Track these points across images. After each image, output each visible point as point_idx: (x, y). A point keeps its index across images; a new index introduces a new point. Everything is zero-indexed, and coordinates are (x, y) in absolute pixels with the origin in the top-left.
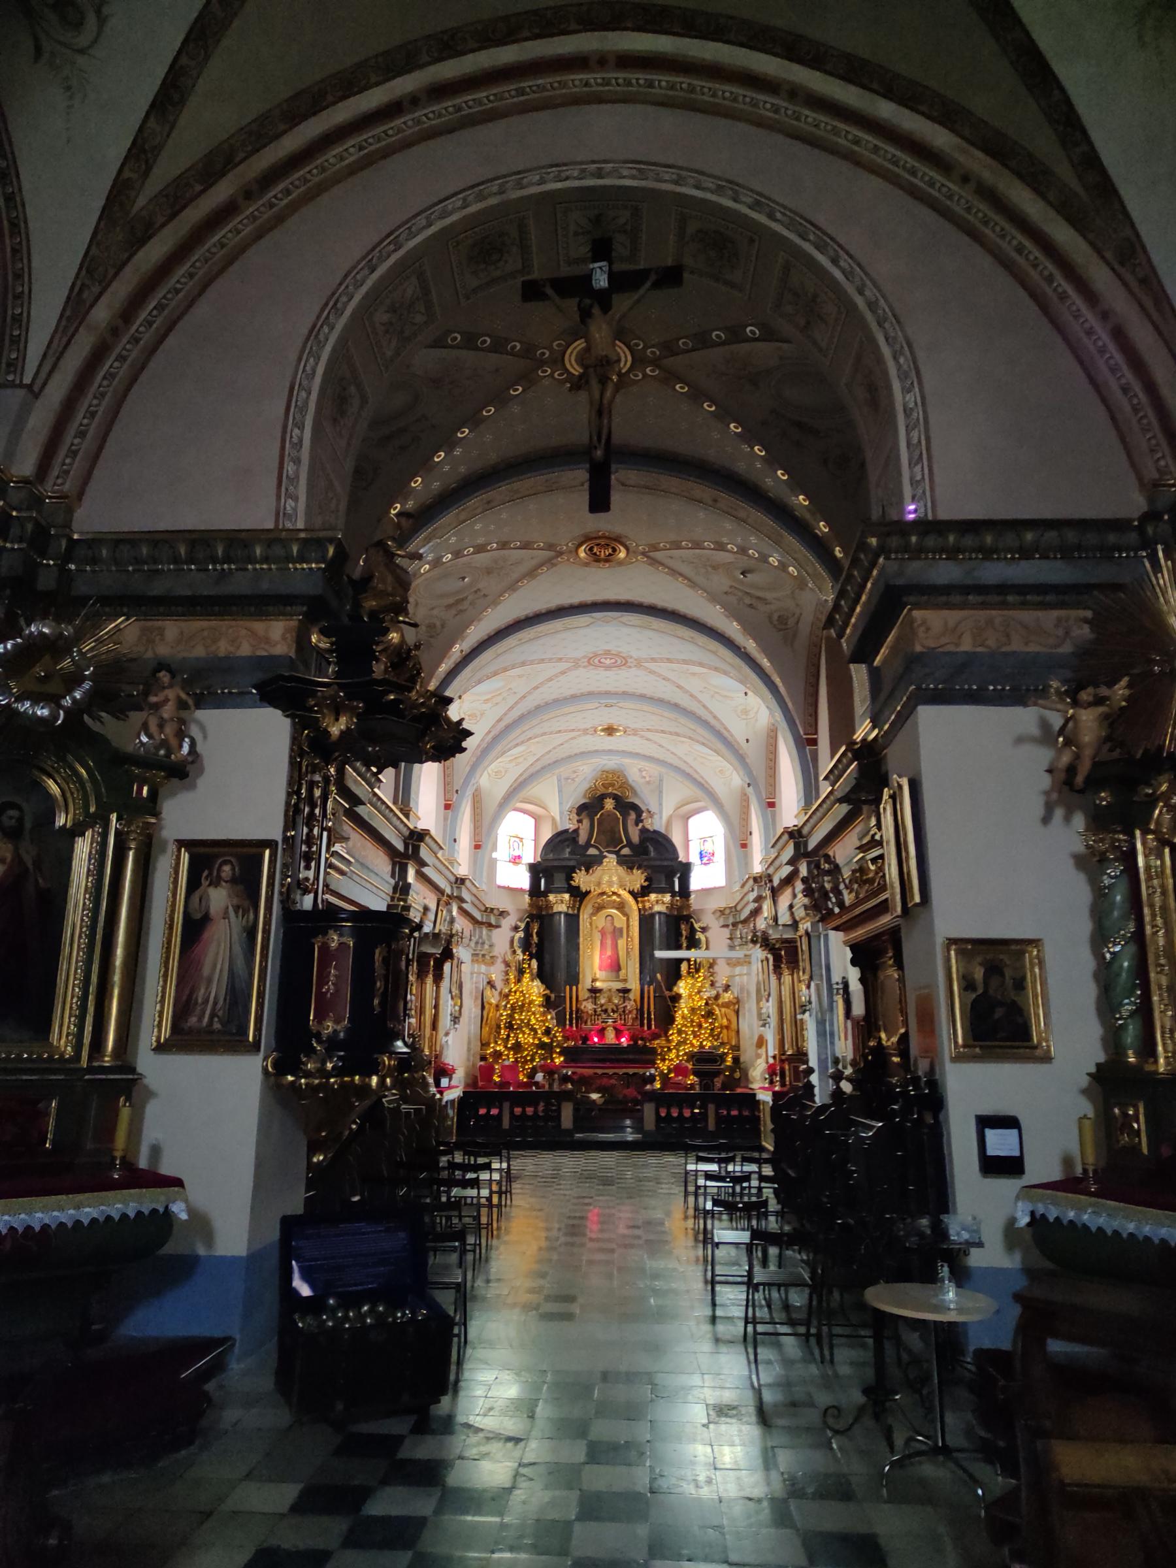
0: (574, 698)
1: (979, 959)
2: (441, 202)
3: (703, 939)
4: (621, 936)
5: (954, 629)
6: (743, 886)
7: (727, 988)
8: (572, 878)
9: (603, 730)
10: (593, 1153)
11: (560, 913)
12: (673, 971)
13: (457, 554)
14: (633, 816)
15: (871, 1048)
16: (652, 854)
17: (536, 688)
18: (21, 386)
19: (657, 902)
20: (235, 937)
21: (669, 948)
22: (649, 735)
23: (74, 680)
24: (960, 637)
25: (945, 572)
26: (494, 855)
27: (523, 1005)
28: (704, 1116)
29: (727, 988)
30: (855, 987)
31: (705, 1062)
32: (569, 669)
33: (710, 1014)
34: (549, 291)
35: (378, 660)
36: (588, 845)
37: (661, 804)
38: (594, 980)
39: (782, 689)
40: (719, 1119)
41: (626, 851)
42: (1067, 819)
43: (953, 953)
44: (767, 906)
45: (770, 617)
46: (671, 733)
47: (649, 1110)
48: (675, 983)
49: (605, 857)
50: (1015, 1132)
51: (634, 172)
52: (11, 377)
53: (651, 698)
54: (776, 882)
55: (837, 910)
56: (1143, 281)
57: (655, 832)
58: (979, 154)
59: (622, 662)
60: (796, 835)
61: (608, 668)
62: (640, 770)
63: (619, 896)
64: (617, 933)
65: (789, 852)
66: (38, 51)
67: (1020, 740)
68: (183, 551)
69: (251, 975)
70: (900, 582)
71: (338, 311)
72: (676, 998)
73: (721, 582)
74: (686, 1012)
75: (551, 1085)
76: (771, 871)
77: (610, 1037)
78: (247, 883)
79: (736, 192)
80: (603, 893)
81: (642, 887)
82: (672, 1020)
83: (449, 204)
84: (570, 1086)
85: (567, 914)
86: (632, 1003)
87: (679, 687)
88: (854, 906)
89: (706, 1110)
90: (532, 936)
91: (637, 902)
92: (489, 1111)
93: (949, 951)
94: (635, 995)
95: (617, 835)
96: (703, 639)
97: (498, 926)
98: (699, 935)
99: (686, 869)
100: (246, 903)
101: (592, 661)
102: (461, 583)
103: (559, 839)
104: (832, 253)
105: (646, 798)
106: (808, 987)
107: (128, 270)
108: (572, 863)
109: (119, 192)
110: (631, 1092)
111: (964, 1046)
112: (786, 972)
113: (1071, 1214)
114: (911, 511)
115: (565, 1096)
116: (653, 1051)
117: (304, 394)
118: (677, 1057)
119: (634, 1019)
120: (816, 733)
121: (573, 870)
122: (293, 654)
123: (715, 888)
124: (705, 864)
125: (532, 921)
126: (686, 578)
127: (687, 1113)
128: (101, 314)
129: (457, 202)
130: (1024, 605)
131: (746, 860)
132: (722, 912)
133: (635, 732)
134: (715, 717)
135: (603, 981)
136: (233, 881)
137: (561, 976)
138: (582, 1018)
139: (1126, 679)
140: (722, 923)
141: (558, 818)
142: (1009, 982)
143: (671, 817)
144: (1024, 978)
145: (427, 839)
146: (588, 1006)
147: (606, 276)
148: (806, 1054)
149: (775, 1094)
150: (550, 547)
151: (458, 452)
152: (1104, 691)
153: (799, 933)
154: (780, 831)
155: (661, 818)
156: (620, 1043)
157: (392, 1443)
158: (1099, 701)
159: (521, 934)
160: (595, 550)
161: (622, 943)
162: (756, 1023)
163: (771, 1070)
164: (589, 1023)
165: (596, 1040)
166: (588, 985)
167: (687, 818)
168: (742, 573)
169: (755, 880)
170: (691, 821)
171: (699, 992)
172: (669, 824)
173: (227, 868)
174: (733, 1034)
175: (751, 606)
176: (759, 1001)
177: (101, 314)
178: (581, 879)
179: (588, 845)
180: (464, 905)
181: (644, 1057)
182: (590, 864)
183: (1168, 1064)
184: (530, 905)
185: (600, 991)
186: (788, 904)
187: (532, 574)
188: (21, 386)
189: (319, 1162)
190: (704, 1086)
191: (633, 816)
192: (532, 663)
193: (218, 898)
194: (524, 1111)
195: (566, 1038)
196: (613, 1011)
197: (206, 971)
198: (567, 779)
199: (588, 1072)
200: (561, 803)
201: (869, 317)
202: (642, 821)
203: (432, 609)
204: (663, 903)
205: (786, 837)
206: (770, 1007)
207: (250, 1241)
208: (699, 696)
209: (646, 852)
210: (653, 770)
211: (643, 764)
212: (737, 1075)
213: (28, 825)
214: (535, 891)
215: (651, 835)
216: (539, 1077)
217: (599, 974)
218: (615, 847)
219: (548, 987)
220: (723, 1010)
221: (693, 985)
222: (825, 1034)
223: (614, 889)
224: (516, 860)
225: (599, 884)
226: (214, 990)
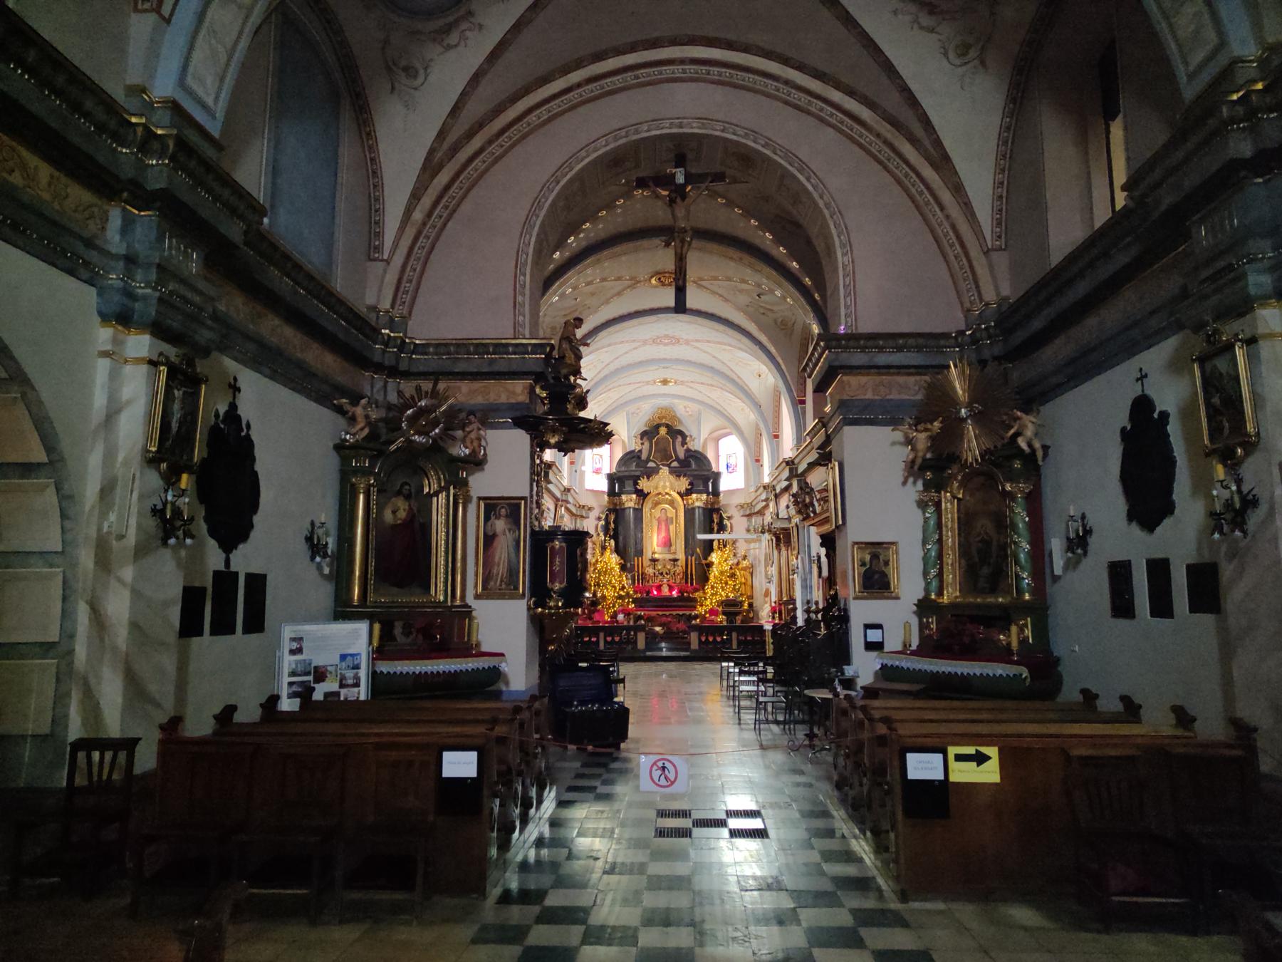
0: (641, 364)
2: (593, 142)
3: (729, 525)
4: (672, 523)
5: (864, 386)
6: (756, 491)
7: (745, 557)
8: (637, 484)
9: (660, 382)
10: (659, 663)
11: (630, 508)
12: (708, 547)
13: (575, 288)
14: (680, 439)
15: (831, 595)
16: (693, 466)
17: (617, 358)
18: (382, 260)
19: (697, 499)
20: (510, 544)
21: (705, 532)
22: (692, 385)
23: (435, 424)
24: (867, 390)
25: (858, 358)
26: (583, 468)
27: (606, 571)
28: (730, 640)
29: (745, 557)
30: (824, 559)
31: (731, 607)
32: (640, 346)
33: (733, 576)
34: (651, 184)
35: (570, 402)
36: (648, 460)
37: (699, 431)
38: (653, 553)
39: (783, 367)
40: (740, 643)
41: (675, 464)
42: (915, 483)
44: (772, 504)
45: (775, 321)
46: (708, 385)
47: (694, 637)
48: (709, 555)
50: (881, 631)
51: (700, 125)
52: (377, 255)
53: (695, 363)
54: (778, 490)
55: (812, 515)
56: (966, 204)
57: (696, 451)
58: (889, 127)
59: (676, 341)
60: (790, 463)
61: (666, 345)
62: (685, 407)
63: (670, 495)
64: (668, 521)
65: (786, 473)
66: (393, 88)
67: (894, 444)
68: (472, 349)
69: (519, 562)
70: (836, 363)
71: (540, 207)
72: (710, 565)
73: (743, 299)
74: (717, 573)
75: (629, 622)
76: (774, 483)
77: (665, 590)
78: (514, 516)
79: (756, 138)
80: (660, 494)
81: (687, 489)
82: (707, 579)
83: (598, 144)
84: (643, 622)
85: (634, 509)
86: (680, 568)
87: (714, 357)
88: (821, 514)
89: (731, 636)
91: (683, 500)
92: (590, 639)
93: (853, 548)
94: (682, 562)
96: (731, 332)
97: (588, 517)
98: (726, 522)
99: (717, 476)
100: (514, 527)
101: (656, 341)
102: (574, 302)
104: (806, 175)
105: (688, 427)
106: (797, 558)
107: (430, 190)
109: (432, 152)
110: (682, 626)
112: (783, 549)
113: (897, 663)
114: (842, 329)
115: (642, 628)
116: (694, 600)
117: (524, 256)
118: (711, 603)
119: (682, 579)
120: (805, 396)
121: (638, 478)
122: (527, 401)
123: (738, 490)
126: (721, 296)
127: (719, 639)
128: (418, 215)
129: (603, 141)
130: (898, 374)
131: (759, 473)
132: (742, 507)
133: (682, 383)
134: (739, 377)
135: (660, 554)
136: (507, 516)
137: (631, 550)
138: (645, 578)
139: (941, 419)
140: (742, 514)
141: (626, 440)
143: (706, 439)
144: (889, 560)
145: (554, 468)
146: (650, 571)
147: (683, 177)
148: (795, 600)
149: (775, 625)
150: (631, 279)
151: (582, 235)
152: (929, 426)
153: (791, 526)
154: (781, 460)
155: (699, 440)
156: (672, 595)
157: (612, 754)
158: (926, 430)
159: (603, 523)
160: (662, 279)
161: (672, 528)
162: (764, 580)
163: (773, 611)
165: (655, 593)
167: (717, 440)
168: (758, 296)
169: (764, 487)
170: (720, 442)
171: (726, 561)
173: (503, 510)
174: (749, 588)
175: (764, 314)
176: (766, 566)
177: (418, 215)
178: (644, 484)
179: (648, 460)
180: (568, 505)
181: (689, 604)
182: (650, 473)
183: (948, 599)
184: (609, 502)
186: (785, 504)
187: (619, 294)
188: (382, 260)
190: (731, 622)
191: (680, 439)
192: (615, 344)
193: (500, 525)
194: (613, 639)
195: (635, 592)
196: (667, 574)
198: (633, 413)
199: (654, 613)
200: (628, 430)
201: (826, 212)
202: (686, 444)
203: (555, 317)
205: (784, 464)
206: (773, 570)
207: (526, 683)
208: (729, 364)
209: (689, 465)
210: (694, 407)
211: (687, 403)
212: (751, 615)
213: (413, 491)
214: (611, 493)
215: (692, 454)
216: (621, 617)
217: (657, 549)
219: (622, 558)
220: (742, 572)
221: (722, 556)
222: (806, 587)
223: (667, 491)
224: (597, 471)
225: (657, 488)
226: (501, 569)
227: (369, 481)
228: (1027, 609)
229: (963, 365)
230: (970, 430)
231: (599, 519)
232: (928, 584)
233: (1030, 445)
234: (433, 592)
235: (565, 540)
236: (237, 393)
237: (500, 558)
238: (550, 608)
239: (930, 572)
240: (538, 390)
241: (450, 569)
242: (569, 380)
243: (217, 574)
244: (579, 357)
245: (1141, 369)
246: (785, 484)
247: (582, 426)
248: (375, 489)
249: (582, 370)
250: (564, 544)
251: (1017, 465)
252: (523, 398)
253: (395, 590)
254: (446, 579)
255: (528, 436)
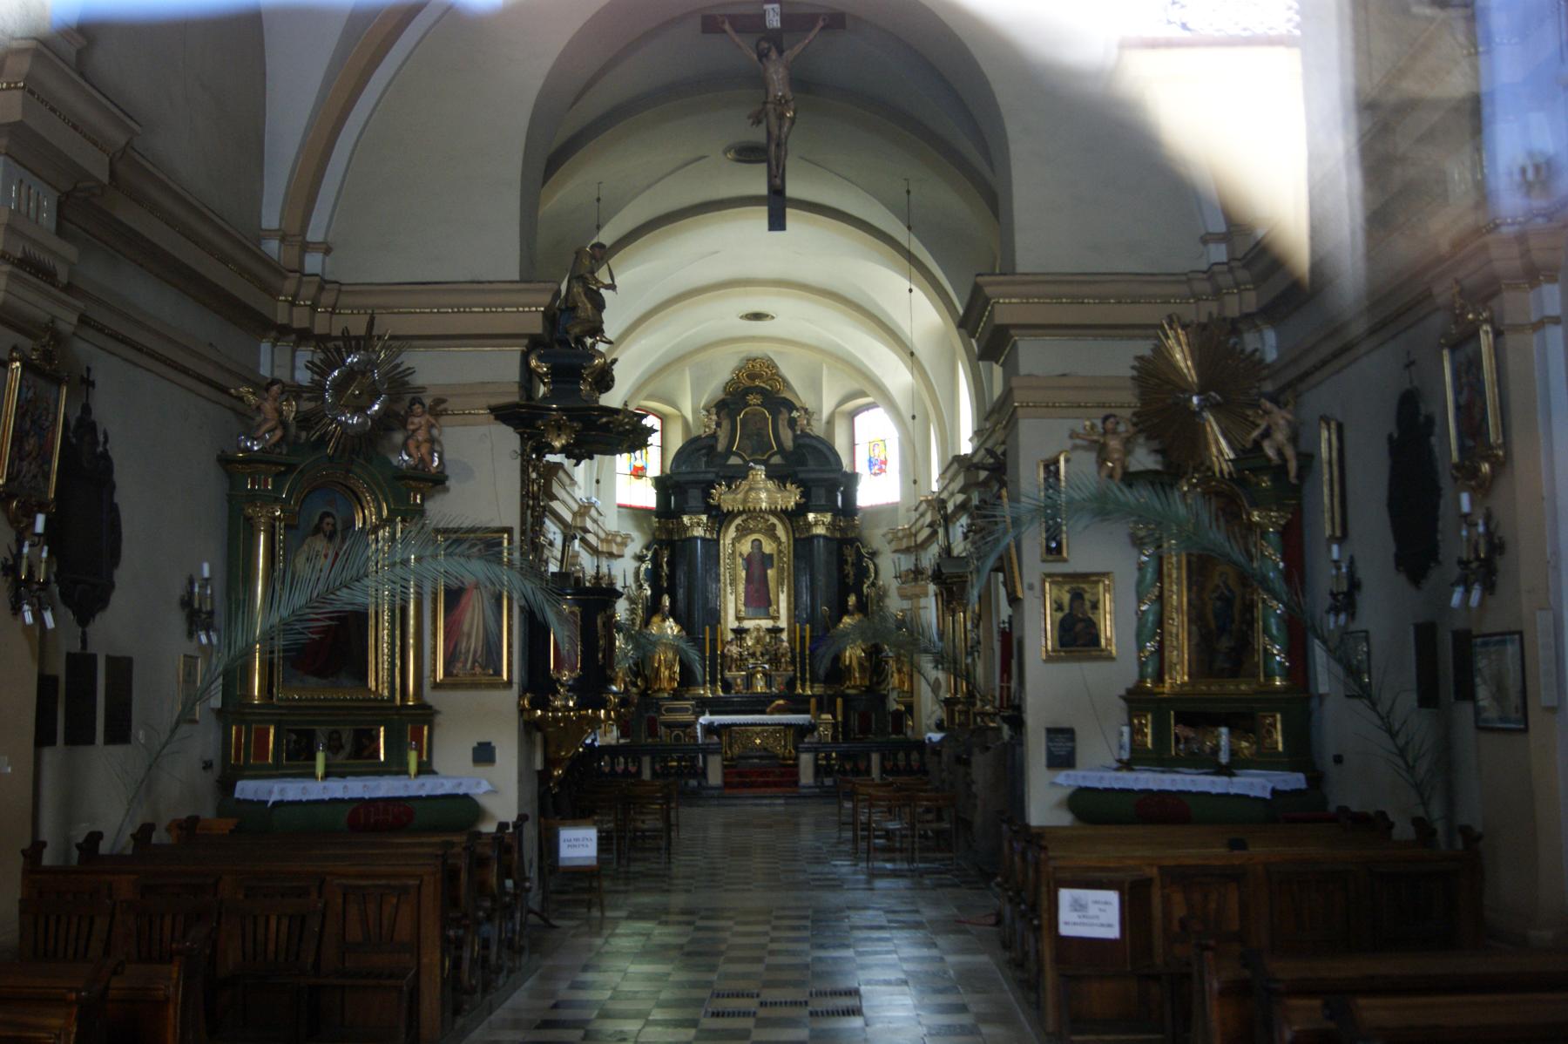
1: (1067, 587)
3: (872, 567)
8: (710, 495)
34: (727, 27)
35: (585, 380)
36: (729, 452)
43: (1047, 585)
44: (941, 531)
49: (752, 468)
54: (950, 507)
64: (767, 560)
76: (944, 496)
85: (703, 539)
90: (662, 566)
95: (766, 439)
97: (621, 556)
99: (852, 479)
103: (693, 447)
108: (710, 476)
111: (1053, 651)
124: (875, 474)
125: (661, 548)
137: (698, 616)
142: (1088, 605)
145: (561, 474)
147: (778, 18)
164: (734, 669)
166: (732, 623)
167: (852, 415)
170: (858, 420)
172: (830, 422)
178: (725, 498)
179: (729, 452)
182: (735, 476)
185: (746, 631)
189: (559, 775)
197: (466, 627)
204: (823, 524)
218: (763, 454)
224: (638, 473)
226: (473, 643)
227: (274, 513)
228: (1272, 700)
229: (1176, 332)
230: (1213, 426)
231: (640, 558)
232: (1142, 665)
233: (1280, 453)
234: (372, 684)
235: (577, 602)
236: (90, 389)
237: (472, 625)
238: (556, 710)
239: (1146, 647)
240: (533, 363)
241: (397, 649)
242: (584, 344)
243: (71, 658)
244: (599, 305)
245: (1408, 353)
246: (960, 498)
247: (604, 420)
248: (282, 525)
249: (605, 327)
250: (576, 609)
251: (1266, 483)
252: (513, 373)
253: (312, 680)
254: (392, 664)
255: (518, 436)
